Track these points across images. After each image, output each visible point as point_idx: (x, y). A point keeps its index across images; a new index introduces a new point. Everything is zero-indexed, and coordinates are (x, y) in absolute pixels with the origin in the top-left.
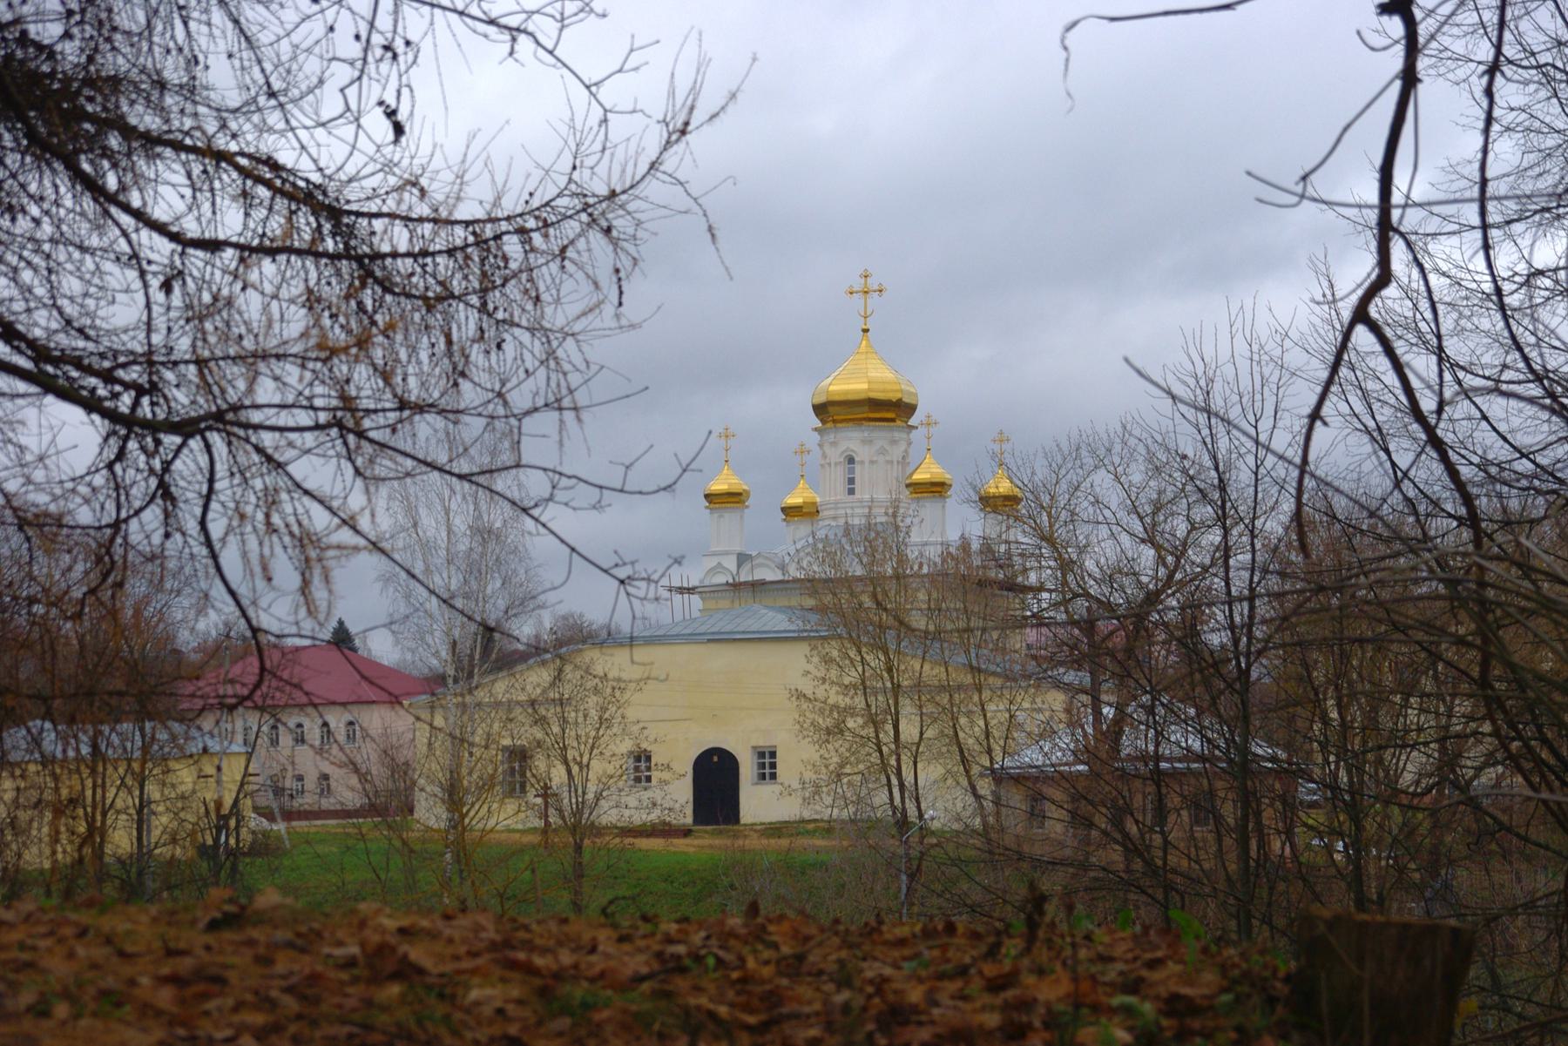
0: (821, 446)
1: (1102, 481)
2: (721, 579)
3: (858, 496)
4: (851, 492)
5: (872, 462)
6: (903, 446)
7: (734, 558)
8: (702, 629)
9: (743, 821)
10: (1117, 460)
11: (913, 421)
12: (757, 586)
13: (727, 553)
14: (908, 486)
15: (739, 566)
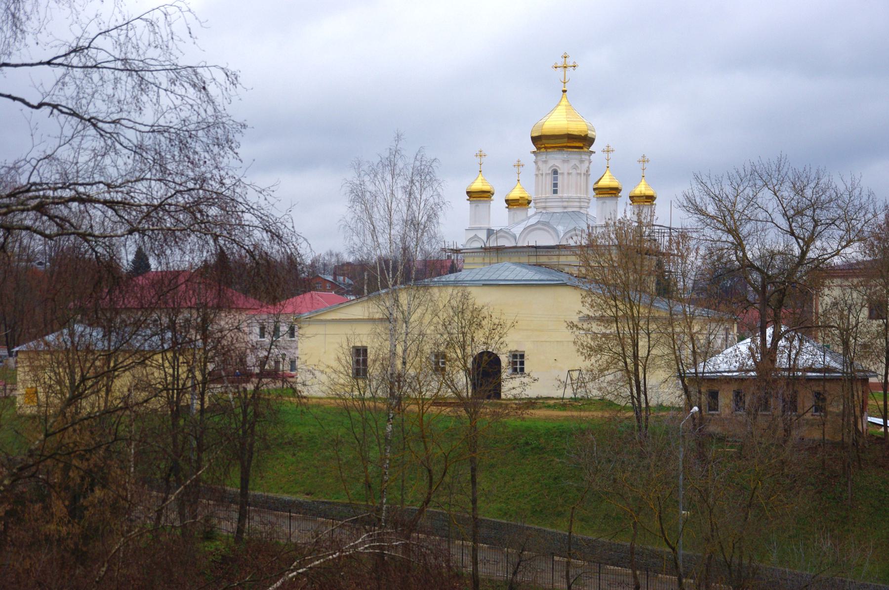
0: (536, 162)
1: (766, 197)
2: (477, 245)
3: (560, 194)
4: (555, 192)
5: (569, 174)
6: (586, 164)
7: (485, 232)
8: (478, 277)
9: (503, 396)
10: (775, 182)
11: (591, 149)
12: (499, 250)
13: (480, 229)
14: (595, 189)
15: (488, 238)
